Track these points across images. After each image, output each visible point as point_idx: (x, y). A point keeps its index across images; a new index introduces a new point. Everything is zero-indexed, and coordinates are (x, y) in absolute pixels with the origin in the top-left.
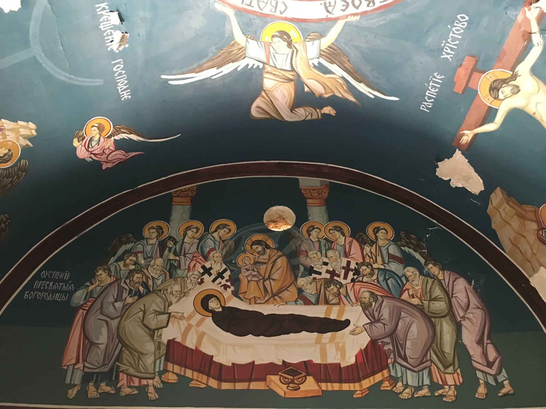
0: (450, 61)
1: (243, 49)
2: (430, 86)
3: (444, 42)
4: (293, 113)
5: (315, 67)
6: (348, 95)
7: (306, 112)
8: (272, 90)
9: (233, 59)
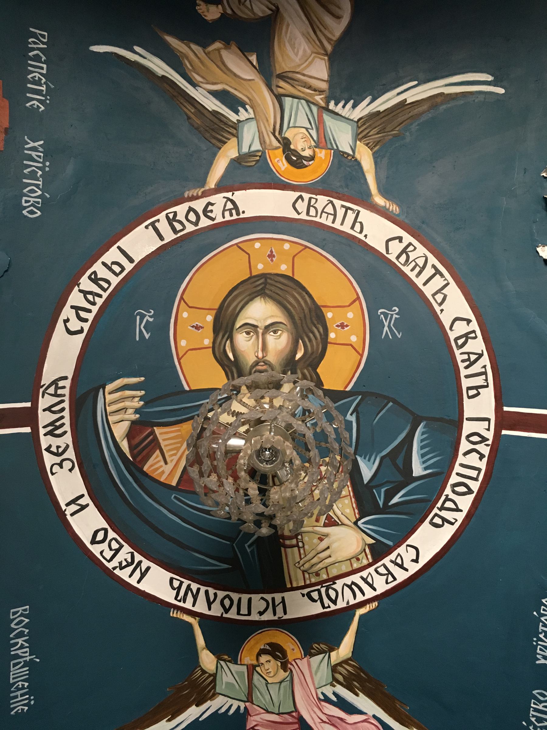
0: (26, 137)
1: (360, 136)
2: (45, 83)
3: (47, 169)
4: (274, 5)
5: (244, 106)
6: (181, 50)
7: (250, 7)
8: (313, 55)
9: (378, 118)
